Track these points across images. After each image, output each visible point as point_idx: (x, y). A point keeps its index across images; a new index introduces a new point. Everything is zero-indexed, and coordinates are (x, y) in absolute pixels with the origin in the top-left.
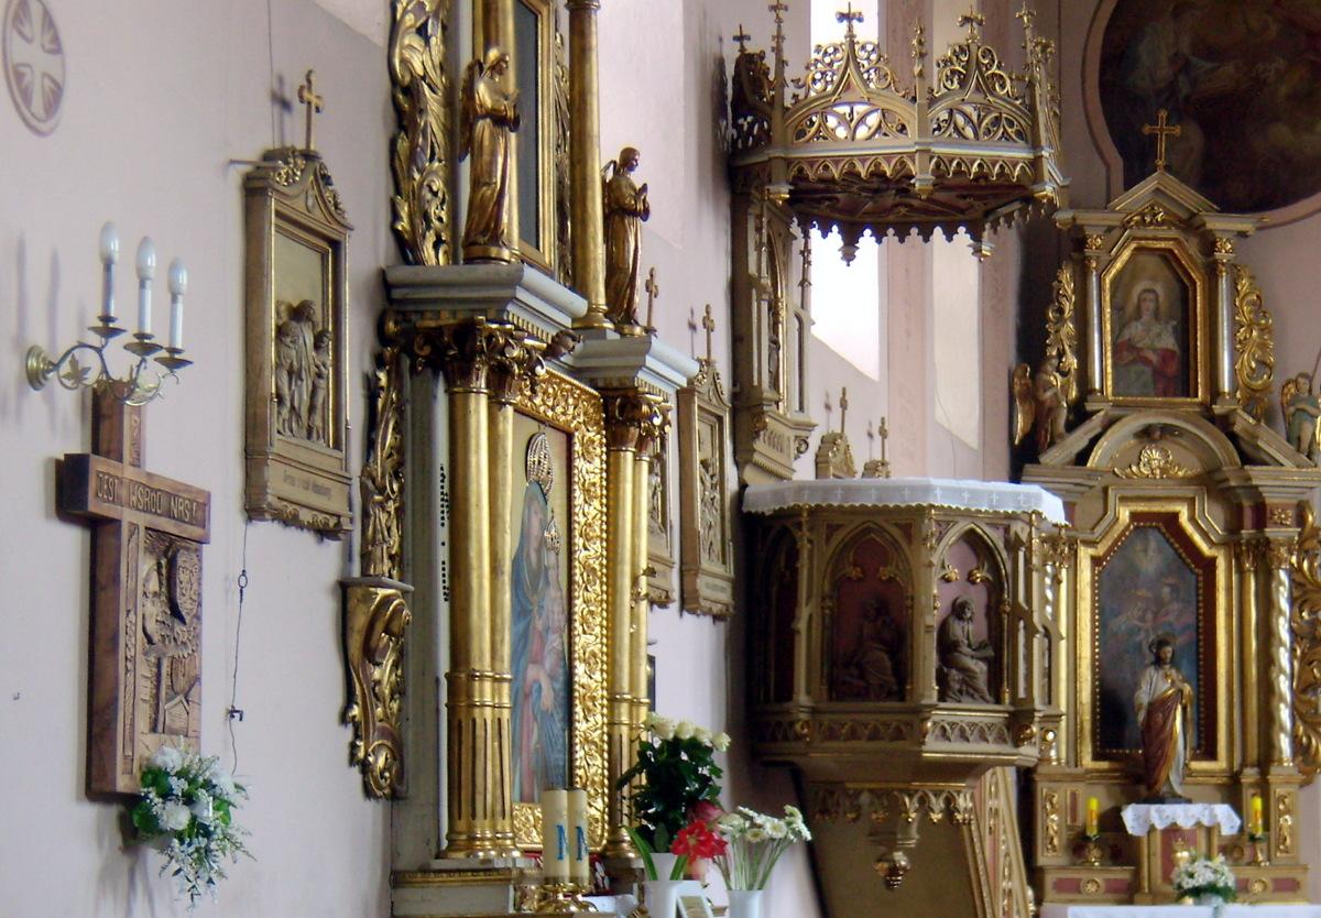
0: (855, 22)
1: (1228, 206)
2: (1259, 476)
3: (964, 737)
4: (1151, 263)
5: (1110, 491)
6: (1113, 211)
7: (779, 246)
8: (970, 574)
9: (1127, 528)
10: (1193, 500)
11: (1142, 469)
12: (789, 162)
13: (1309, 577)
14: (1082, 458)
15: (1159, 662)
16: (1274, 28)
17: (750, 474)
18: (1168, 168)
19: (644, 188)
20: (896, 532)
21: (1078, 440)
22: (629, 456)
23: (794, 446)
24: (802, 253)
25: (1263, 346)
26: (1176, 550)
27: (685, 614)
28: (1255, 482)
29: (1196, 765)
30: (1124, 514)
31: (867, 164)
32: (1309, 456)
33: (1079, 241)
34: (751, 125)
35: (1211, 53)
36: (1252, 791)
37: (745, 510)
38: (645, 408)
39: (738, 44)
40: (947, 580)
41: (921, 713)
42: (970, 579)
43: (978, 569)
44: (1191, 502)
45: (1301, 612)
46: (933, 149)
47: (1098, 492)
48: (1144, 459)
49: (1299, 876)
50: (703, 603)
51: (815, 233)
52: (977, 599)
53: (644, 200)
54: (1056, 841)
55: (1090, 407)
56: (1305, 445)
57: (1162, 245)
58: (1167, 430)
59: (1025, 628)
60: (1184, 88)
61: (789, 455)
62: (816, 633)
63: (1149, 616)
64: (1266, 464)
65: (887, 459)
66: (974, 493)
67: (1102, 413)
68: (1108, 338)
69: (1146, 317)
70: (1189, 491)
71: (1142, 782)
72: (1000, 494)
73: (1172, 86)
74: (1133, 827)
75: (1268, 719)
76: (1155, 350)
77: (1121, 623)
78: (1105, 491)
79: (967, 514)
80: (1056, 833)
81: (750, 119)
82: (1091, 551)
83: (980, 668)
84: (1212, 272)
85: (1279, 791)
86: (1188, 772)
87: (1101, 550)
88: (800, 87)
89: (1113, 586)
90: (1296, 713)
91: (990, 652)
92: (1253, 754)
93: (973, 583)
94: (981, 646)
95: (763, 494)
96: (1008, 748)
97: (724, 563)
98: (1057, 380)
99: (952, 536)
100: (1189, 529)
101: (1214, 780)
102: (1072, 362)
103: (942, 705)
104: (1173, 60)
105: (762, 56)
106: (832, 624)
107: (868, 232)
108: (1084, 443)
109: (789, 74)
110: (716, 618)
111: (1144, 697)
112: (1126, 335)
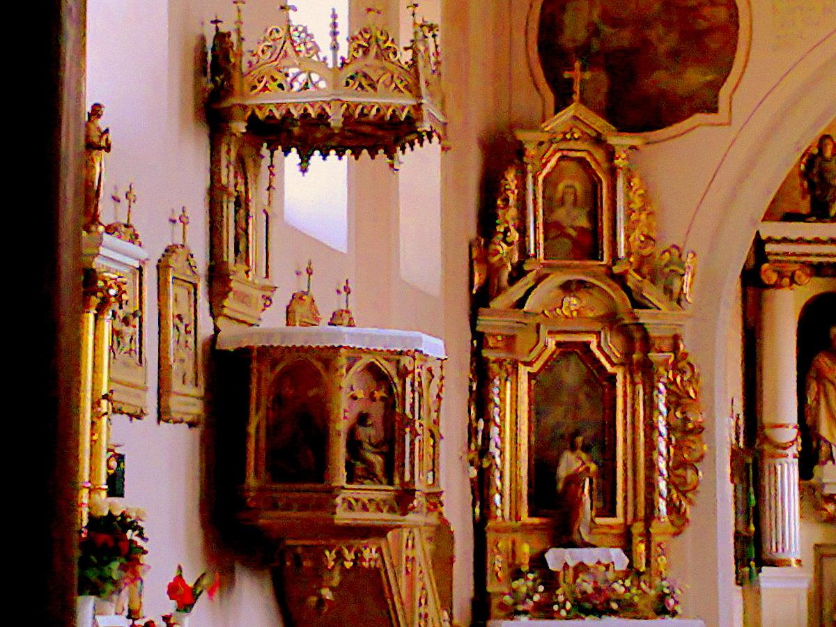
0: (291, 12)
2: (644, 316)
3: (365, 508)
4: (572, 167)
5: (542, 326)
6: (542, 131)
7: (250, 164)
8: (372, 394)
9: (554, 353)
10: (600, 332)
11: (564, 311)
12: (245, 108)
13: (681, 388)
14: (520, 303)
15: (573, 449)
17: (221, 322)
18: (583, 101)
19: (107, 131)
20: (319, 366)
22: (91, 317)
23: (261, 302)
24: (269, 167)
25: (649, 226)
26: (589, 368)
27: (162, 423)
28: (641, 321)
31: (299, 108)
32: (679, 301)
33: (520, 150)
34: (223, 81)
36: (640, 539)
37: (217, 347)
38: (100, 284)
39: (214, 26)
40: (354, 398)
41: (332, 492)
42: (372, 398)
43: (377, 390)
44: (598, 334)
45: (675, 411)
46: (342, 98)
47: (533, 329)
48: (565, 304)
50: (173, 414)
51: (279, 152)
52: (377, 411)
53: (107, 140)
54: (500, 574)
55: (526, 268)
56: (675, 296)
57: (579, 154)
58: (581, 285)
59: (411, 432)
60: (596, 45)
61: (257, 308)
62: (263, 433)
64: (648, 308)
65: (349, 308)
66: (372, 337)
67: (534, 272)
70: (598, 327)
71: (563, 535)
72: (392, 337)
74: (553, 565)
75: (651, 486)
76: (575, 228)
77: (550, 421)
78: (538, 326)
79: (368, 351)
80: (500, 568)
81: (222, 77)
82: (528, 369)
83: (377, 460)
84: (613, 172)
85: (657, 539)
86: (593, 526)
87: (535, 368)
88: (254, 56)
89: (542, 397)
90: (669, 483)
91: (384, 449)
92: (642, 514)
95: (232, 337)
96: (396, 516)
97: (196, 385)
98: (503, 249)
99: (359, 366)
100: (598, 354)
101: (615, 531)
102: (514, 236)
103: (349, 486)
105: (229, 35)
106: (273, 429)
107: (317, 153)
108: (521, 294)
109: (246, 46)
110: (191, 425)
111: (562, 472)
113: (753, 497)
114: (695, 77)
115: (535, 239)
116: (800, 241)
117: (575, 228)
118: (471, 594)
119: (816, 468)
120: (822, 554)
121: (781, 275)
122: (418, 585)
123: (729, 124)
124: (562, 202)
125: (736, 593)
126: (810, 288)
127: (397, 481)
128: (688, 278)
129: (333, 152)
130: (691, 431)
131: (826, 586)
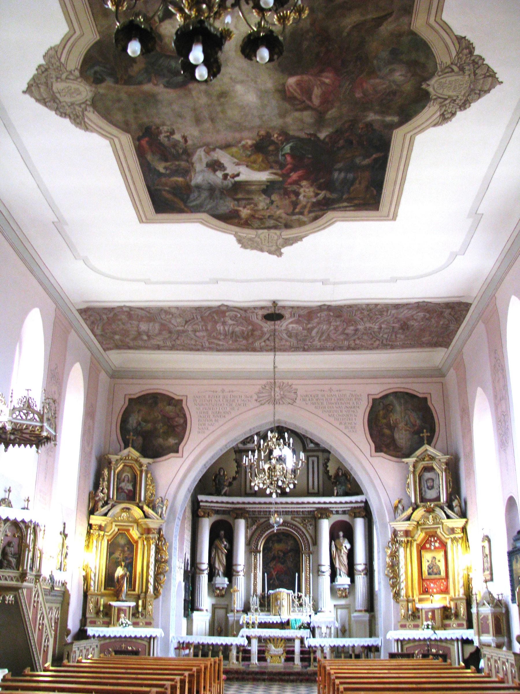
1: (145, 456)
3: (6, 579)
4: (127, 469)
16: (160, 417)
21: (105, 509)
29: (129, 592)
30: (117, 530)
35: (145, 421)
40: (6, 535)
49: (152, 622)
52: (15, 542)
63: (122, 554)
68: (115, 486)
69: (126, 482)
71: (117, 596)
73: (136, 428)
83: (13, 561)
93: (15, 537)
94: (15, 554)
98: (101, 495)
102: (106, 491)
104: (137, 422)
107: (11, 445)
112: (121, 485)
113: (191, 588)
114: (172, 441)
115: (113, 493)
116: (212, 502)
117: (127, 490)
118: (81, 617)
119: (214, 578)
120: (214, 608)
121: (204, 513)
122: (39, 612)
123: (182, 457)
124: (124, 481)
125: (184, 621)
126: (215, 518)
127: (21, 569)
128: (164, 508)
129: (17, 445)
130: (163, 562)
131: (216, 618)
